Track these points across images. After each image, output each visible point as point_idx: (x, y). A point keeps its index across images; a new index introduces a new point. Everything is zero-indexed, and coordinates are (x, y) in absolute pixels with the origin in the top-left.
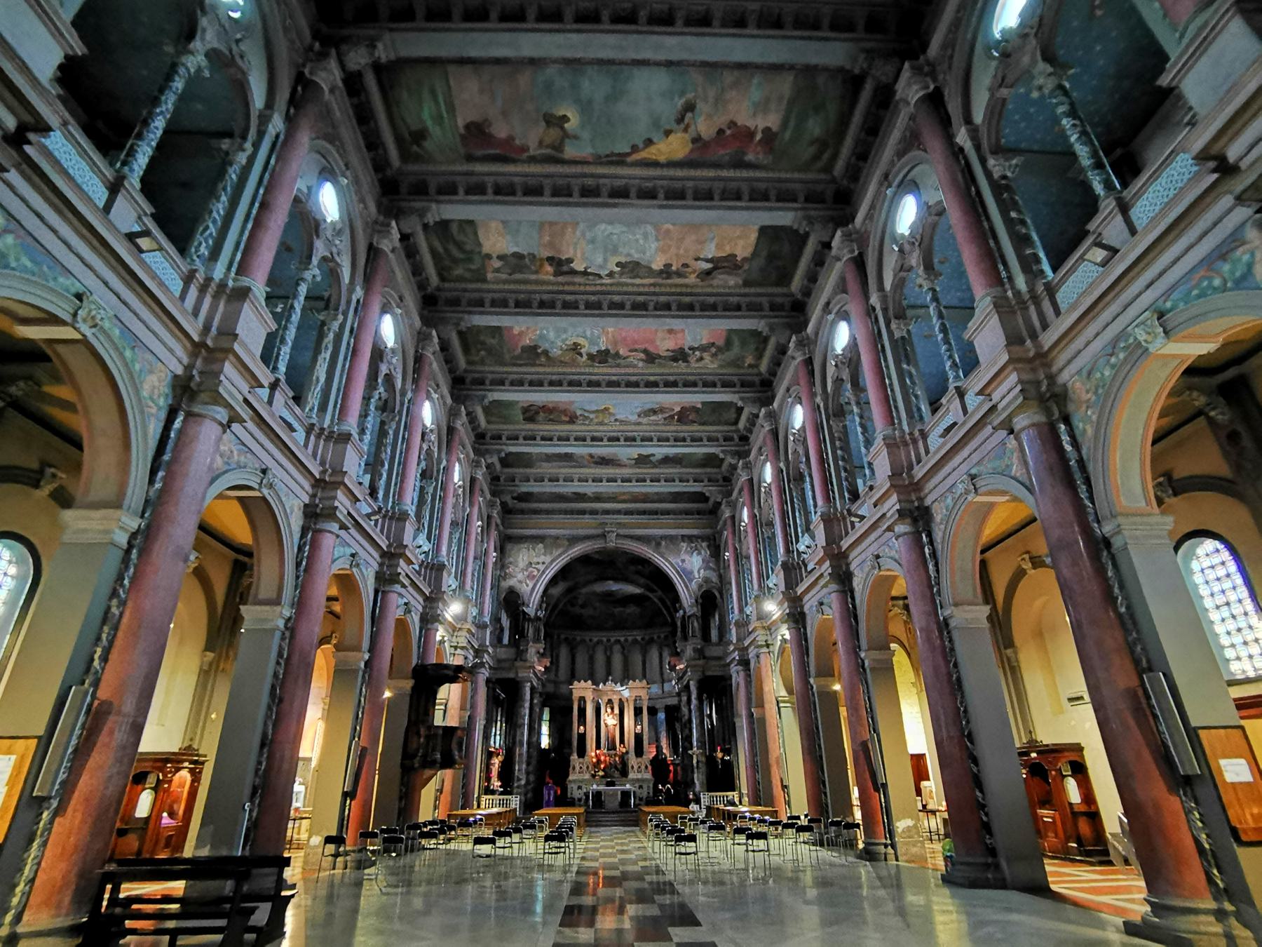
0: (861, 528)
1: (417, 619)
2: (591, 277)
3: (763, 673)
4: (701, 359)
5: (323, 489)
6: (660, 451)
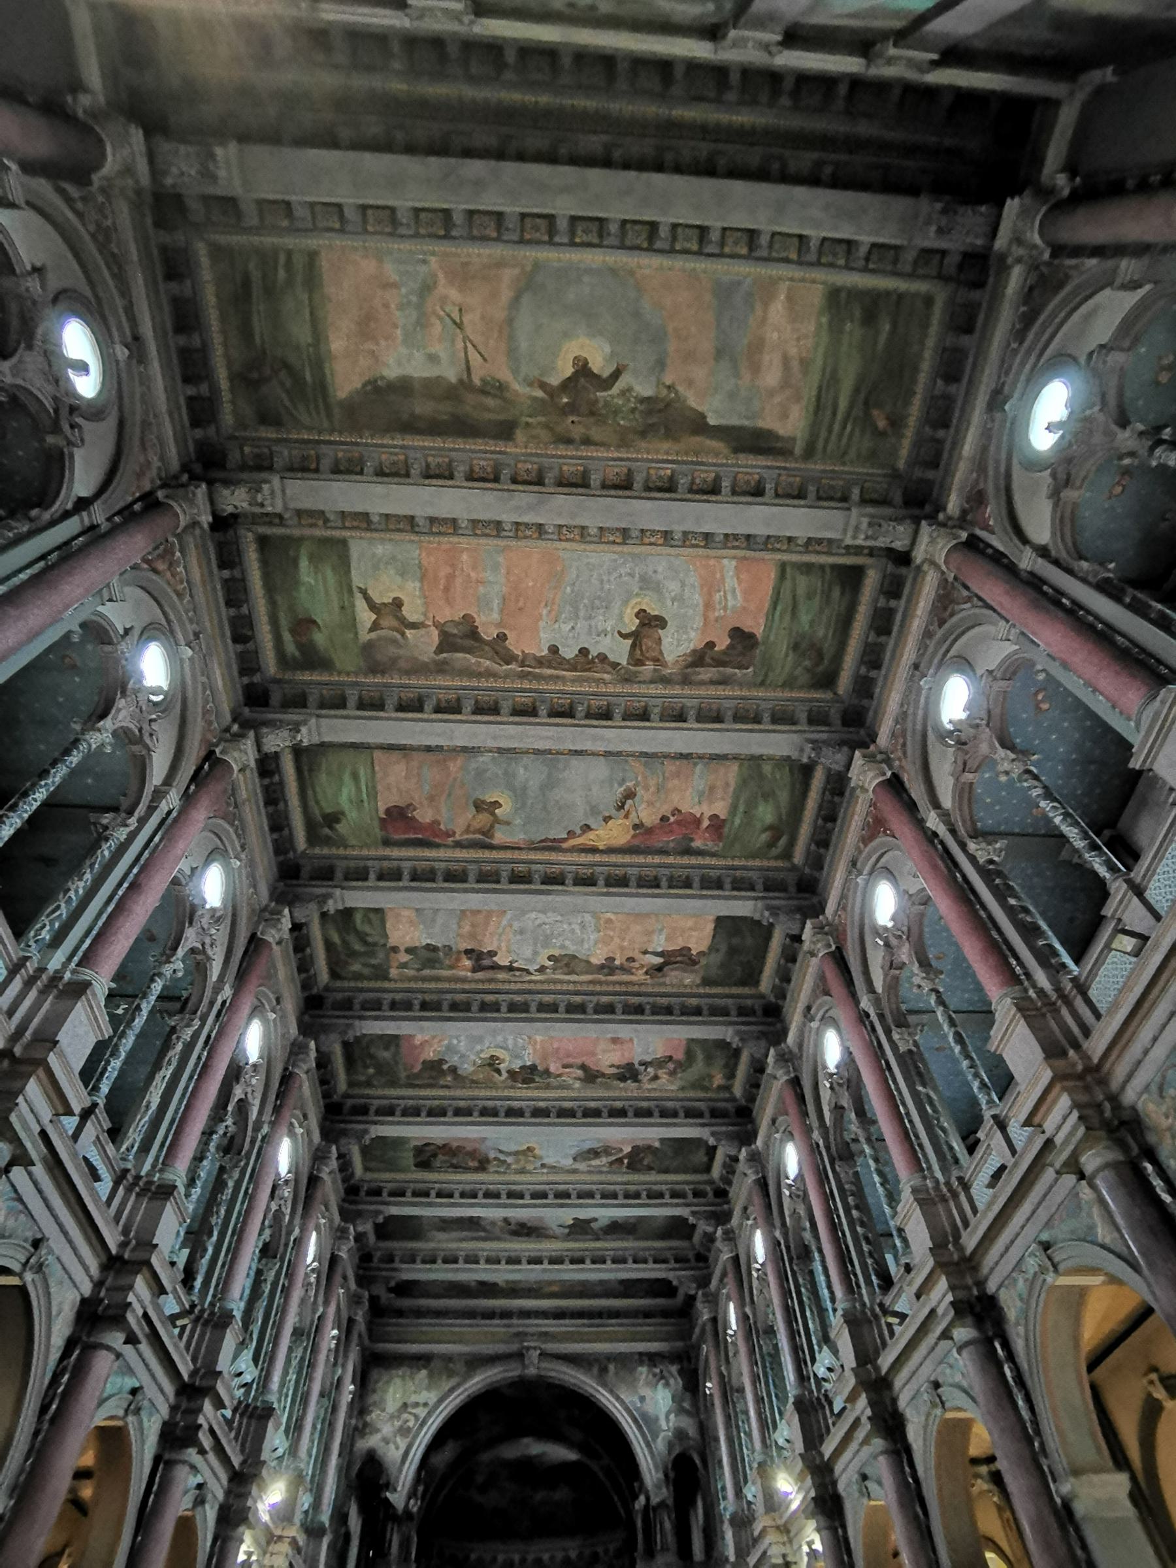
0: (904, 1333)
4: (656, 1078)
6: (605, 1214)
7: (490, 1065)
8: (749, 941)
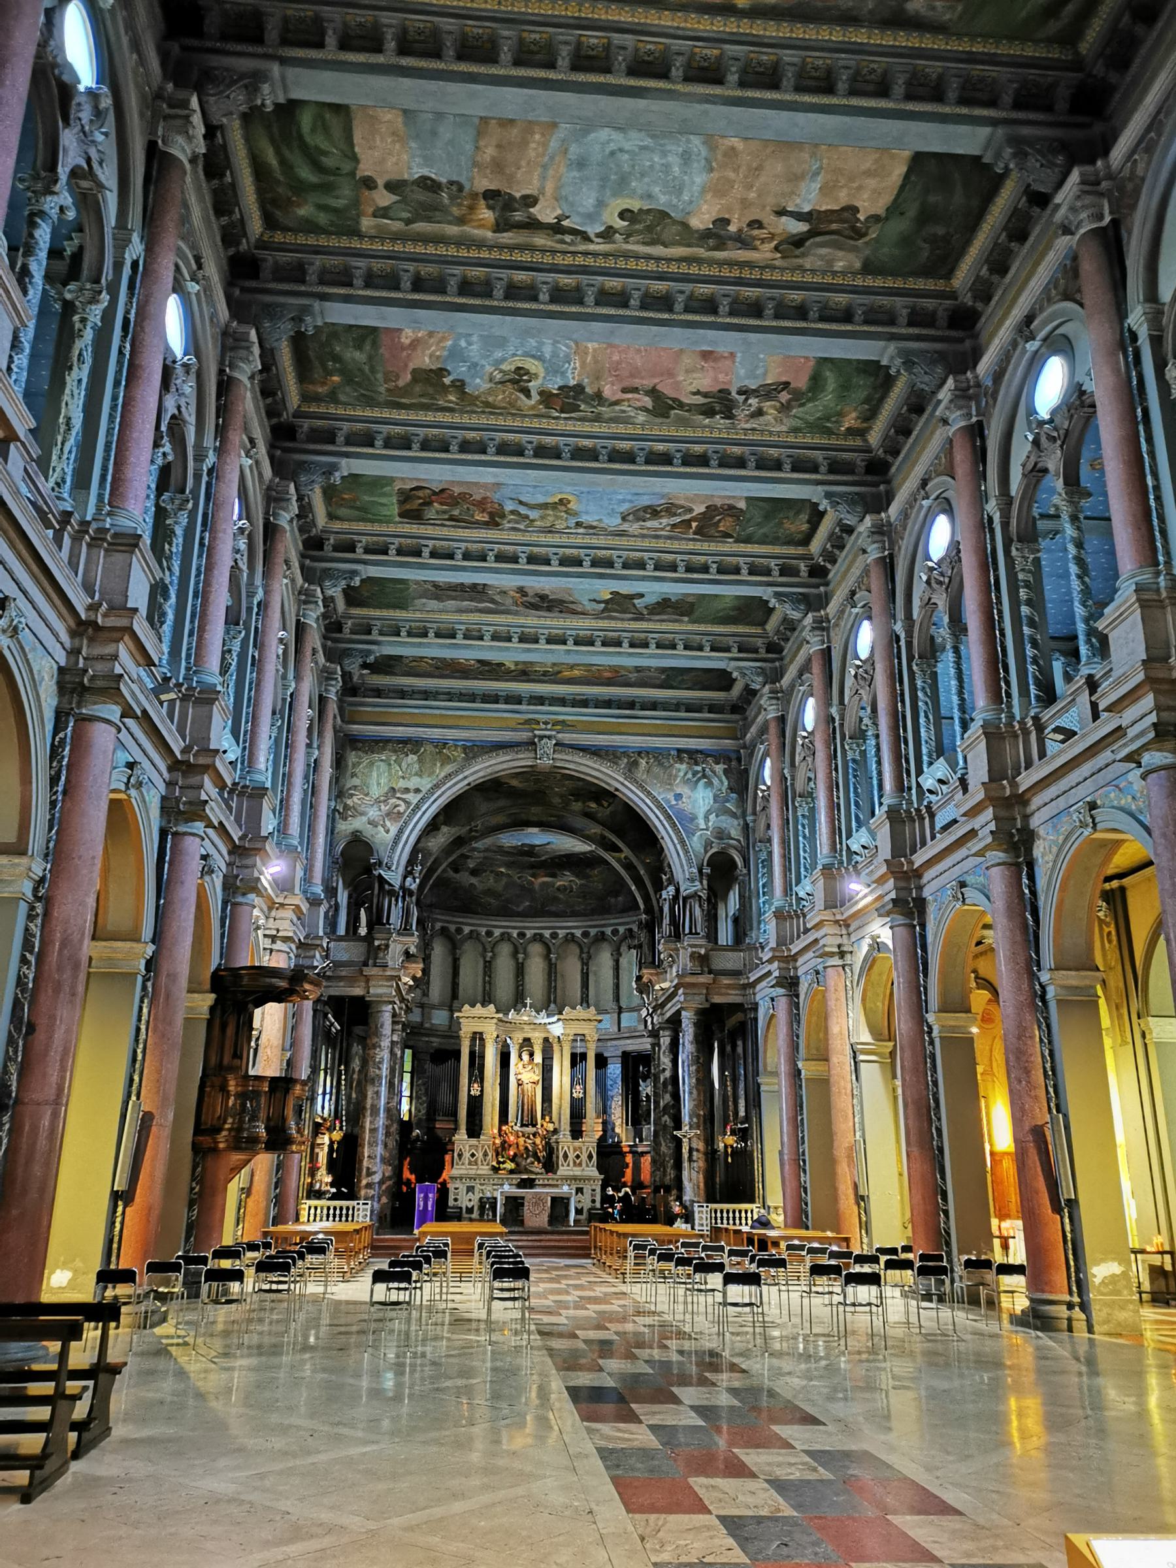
0: (1058, 752)
1: (218, 881)
2: (568, 238)
3: (832, 1003)
4: (759, 413)
5: (91, 640)
6: (653, 590)
7: (514, 382)
8: (958, 198)
